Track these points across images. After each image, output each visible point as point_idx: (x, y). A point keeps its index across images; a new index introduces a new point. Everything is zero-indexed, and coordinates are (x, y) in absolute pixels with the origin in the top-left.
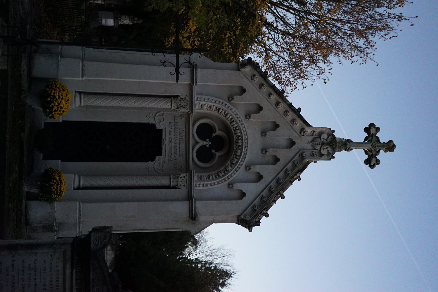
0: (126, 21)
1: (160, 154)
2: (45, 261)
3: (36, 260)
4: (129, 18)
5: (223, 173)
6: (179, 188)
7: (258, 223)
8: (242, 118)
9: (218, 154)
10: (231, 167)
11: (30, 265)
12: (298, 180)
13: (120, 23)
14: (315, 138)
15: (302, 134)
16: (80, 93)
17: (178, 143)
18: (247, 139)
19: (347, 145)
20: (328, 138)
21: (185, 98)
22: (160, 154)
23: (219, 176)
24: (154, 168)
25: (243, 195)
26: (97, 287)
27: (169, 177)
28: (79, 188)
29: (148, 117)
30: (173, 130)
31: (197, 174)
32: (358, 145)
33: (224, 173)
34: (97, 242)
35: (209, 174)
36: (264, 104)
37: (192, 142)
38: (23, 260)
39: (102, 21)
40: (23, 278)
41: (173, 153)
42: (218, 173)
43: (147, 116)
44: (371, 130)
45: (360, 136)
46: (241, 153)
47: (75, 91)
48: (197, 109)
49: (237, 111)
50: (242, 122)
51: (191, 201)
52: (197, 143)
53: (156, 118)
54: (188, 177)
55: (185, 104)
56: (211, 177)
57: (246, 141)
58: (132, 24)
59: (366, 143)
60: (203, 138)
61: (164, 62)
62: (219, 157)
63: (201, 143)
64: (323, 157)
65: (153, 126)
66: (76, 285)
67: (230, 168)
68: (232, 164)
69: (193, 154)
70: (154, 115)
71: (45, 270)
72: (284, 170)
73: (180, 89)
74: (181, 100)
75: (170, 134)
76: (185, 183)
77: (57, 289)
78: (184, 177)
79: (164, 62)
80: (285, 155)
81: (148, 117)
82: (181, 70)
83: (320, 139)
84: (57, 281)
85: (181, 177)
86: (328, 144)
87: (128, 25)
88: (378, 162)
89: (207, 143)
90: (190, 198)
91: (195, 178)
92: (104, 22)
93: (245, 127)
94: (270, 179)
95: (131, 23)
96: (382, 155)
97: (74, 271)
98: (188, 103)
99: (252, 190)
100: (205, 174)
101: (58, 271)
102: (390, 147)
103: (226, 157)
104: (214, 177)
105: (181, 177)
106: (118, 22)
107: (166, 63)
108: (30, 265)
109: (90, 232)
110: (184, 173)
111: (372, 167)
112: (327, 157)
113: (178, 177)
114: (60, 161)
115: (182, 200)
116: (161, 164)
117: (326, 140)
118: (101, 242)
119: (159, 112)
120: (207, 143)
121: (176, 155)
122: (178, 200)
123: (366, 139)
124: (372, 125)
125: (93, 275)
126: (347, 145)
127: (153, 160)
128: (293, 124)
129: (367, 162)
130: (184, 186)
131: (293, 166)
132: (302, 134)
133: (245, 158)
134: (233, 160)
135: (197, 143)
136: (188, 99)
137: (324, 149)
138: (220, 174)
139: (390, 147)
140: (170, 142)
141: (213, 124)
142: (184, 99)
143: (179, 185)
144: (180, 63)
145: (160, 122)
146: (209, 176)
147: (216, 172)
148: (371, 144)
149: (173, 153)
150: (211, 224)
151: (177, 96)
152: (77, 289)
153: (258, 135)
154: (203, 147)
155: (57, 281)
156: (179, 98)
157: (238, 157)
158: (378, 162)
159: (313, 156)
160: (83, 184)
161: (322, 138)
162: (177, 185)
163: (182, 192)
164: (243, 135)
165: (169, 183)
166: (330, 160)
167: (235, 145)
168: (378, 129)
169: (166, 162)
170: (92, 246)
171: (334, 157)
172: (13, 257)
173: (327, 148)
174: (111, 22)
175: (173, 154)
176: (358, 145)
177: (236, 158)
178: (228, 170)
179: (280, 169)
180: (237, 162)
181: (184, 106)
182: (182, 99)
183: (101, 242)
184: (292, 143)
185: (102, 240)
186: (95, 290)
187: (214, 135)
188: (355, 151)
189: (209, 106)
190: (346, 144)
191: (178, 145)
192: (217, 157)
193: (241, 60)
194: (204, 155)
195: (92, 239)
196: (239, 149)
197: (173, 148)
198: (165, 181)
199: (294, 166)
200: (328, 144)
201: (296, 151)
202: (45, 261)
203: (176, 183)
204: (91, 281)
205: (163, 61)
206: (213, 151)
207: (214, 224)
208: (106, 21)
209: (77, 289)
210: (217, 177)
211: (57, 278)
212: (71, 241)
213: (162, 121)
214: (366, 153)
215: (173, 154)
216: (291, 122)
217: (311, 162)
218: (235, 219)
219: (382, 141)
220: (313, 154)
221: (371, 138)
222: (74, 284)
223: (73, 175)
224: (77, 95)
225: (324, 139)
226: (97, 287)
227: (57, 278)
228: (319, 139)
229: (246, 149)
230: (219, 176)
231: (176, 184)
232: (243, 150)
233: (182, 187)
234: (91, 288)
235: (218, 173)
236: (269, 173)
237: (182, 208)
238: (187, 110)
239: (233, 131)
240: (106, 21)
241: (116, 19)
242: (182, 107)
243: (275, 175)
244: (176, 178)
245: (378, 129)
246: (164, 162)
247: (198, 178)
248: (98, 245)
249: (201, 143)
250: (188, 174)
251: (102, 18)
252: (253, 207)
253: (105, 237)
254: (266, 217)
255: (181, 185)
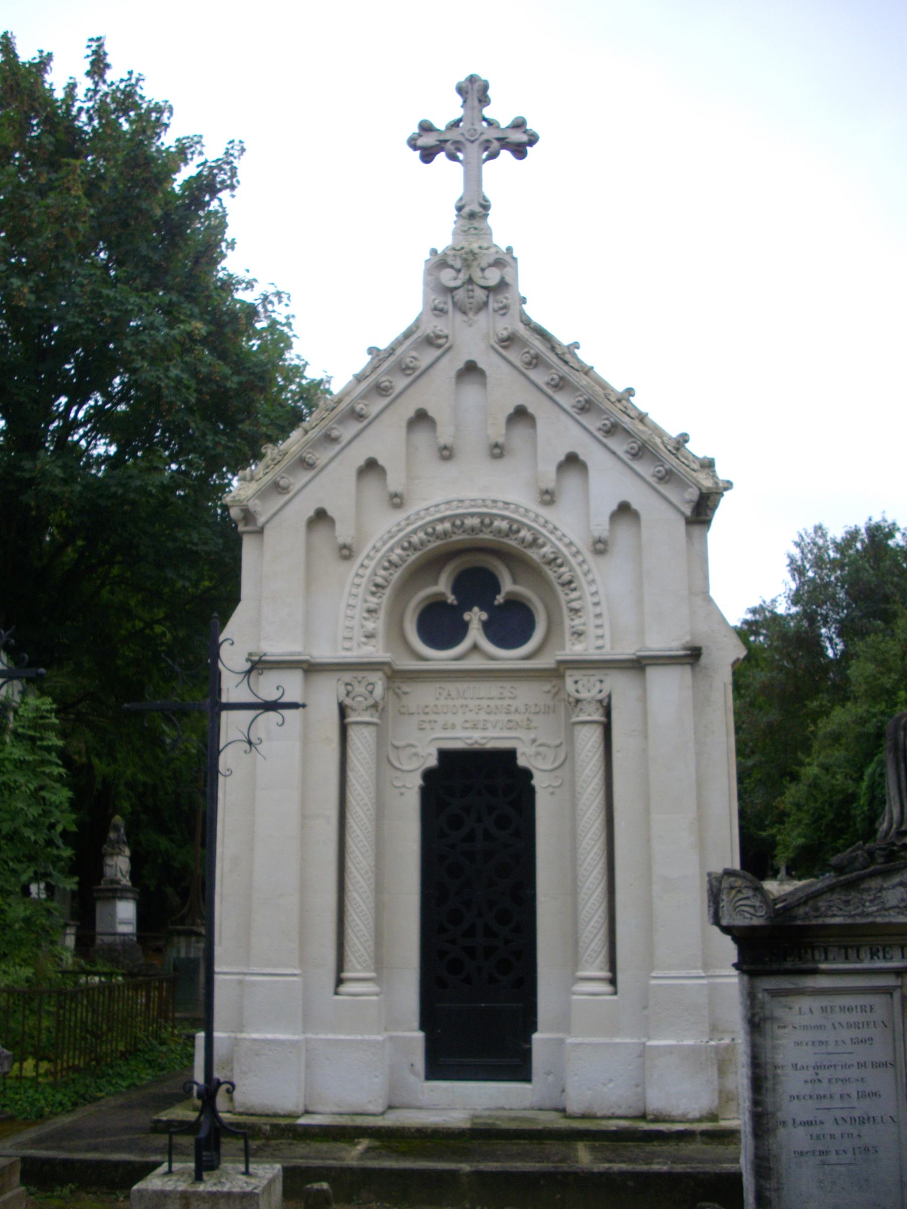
0: (120, 865)
1: (511, 754)
2: (798, 1044)
3: (795, 1067)
4: (112, 855)
5: (563, 569)
6: (609, 697)
7: (708, 465)
8: (399, 516)
9: (508, 586)
10: (543, 546)
11: (806, 1082)
12: (578, 348)
13: (126, 881)
14: (455, 304)
15: (441, 341)
16: (340, 981)
17: (478, 702)
18: (462, 501)
19: (473, 212)
20: (452, 267)
21: (347, 684)
22: (511, 754)
23: (570, 582)
24: (551, 771)
25: (624, 510)
26: (867, 904)
27: (578, 727)
28: (613, 981)
29: (403, 790)
30: (441, 719)
31: (568, 644)
32: (473, 180)
33: (561, 566)
34: (743, 908)
35: (565, 611)
36: (357, 456)
37: (475, 663)
38: (792, 1097)
39: (124, 935)
40: (841, 1096)
41: (505, 718)
42: (563, 585)
43: (402, 794)
44: (429, 145)
45: (447, 173)
46: (504, 518)
47: (336, 993)
48: (375, 651)
49: (382, 533)
50: (412, 518)
51: (644, 662)
52: (475, 647)
53: (405, 767)
54: (575, 672)
55: (364, 683)
56: (576, 605)
57: (467, 503)
58: (129, 847)
59: (466, 157)
60: (459, 631)
61: (250, 743)
62: (515, 582)
63: (475, 634)
64: (508, 279)
65: (428, 775)
66: (861, 961)
67: (546, 550)
68: (534, 543)
69: (510, 657)
70: (399, 774)
71: (821, 1043)
72: (550, 391)
73: (326, 695)
74: (351, 695)
75: (453, 726)
76: (592, 679)
77: (871, 1008)
78: (576, 682)
79: (250, 743)
80: (506, 387)
81: (403, 790)
82: (270, 695)
83: (456, 288)
84: (850, 1009)
85: (577, 691)
86: (472, 278)
87: (133, 860)
88: (519, 124)
89: (476, 617)
90: (638, 665)
91: (575, 650)
92: (129, 929)
93: (427, 509)
94: (576, 430)
95: (127, 852)
96: (500, 112)
97: (823, 966)
98: (360, 675)
99: (610, 481)
100: (567, 623)
101: (824, 1009)
102: (474, 91)
103: (515, 560)
104: (574, 595)
105: (577, 691)
106: (125, 889)
107: (253, 740)
108: (806, 1082)
109: (726, 930)
110: (564, 684)
111: (533, 140)
112: (508, 269)
113: (578, 701)
114: (536, 1036)
115: (644, 689)
116: (541, 749)
117: (459, 271)
118: (747, 898)
119: (389, 761)
120: (476, 617)
121: (513, 709)
122: (643, 699)
123: (453, 157)
124: (413, 144)
125: (834, 916)
126: (473, 212)
127: (527, 775)
128: (414, 369)
129: (519, 151)
130: (601, 681)
131: (536, 366)
132: (441, 341)
133: (518, 506)
134: (523, 540)
135: (475, 647)
136: (347, 677)
137: (484, 278)
138: (566, 577)
139: (474, 91)
140: (475, 727)
141: (418, 605)
142: (349, 688)
143: (600, 696)
144: (248, 698)
145: (416, 754)
146: (572, 610)
147: (559, 589)
148: (468, 145)
149: (505, 718)
150: (710, 600)
151: (343, 711)
152: (872, 958)
153: (449, 470)
154: (487, 627)
155: (850, 1009)
156: (348, 702)
157: (515, 527)
158: (519, 124)
159: (505, 307)
160: (601, 969)
161: (452, 284)
162: (601, 701)
163: (620, 687)
164: (448, 513)
165: (595, 726)
166: (515, 259)
167: (481, 536)
168: (426, 128)
169: (532, 736)
170: (756, 922)
171: (509, 250)
172: (784, 1123)
173: (483, 270)
174: (126, 912)
175: (512, 717)
176: (473, 180)
177: (518, 531)
178: (552, 556)
179: (548, 404)
180: (530, 528)
181: (370, 687)
182: (348, 694)
183: (747, 898)
184: (471, 370)
185: (741, 896)
186: (874, 908)
187: (451, 599)
188: (488, 190)
189: (366, 615)
190: (472, 216)
191: (485, 703)
192: (519, 589)
193: (93, 472)
194: (511, 624)
195: (740, 921)
196: (491, 523)
197: (492, 718)
198: (589, 740)
199: (536, 361)
200: (472, 278)
201: (495, 358)
202: (798, 1044)
203: (594, 706)
204: (849, 921)
205: (247, 746)
206: (500, 599)
207: (713, 593)
208: (124, 923)
209: (872, 958)
210: (573, 586)
211: (842, 1009)
212: (746, 978)
213: (413, 750)
214: (493, 156)
215: (512, 717)
216: (409, 375)
217: (522, 314)
218: (696, 530)
219: (458, 113)
220: (501, 309)
221: (448, 144)
222: (858, 966)
223: (575, 997)
224: (344, 988)
225: (455, 279)
226: (867, 904)
227: (842, 1009)
228: (456, 292)
229: (489, 503)
230: (570, 582)
231: (598, 705)
232: (495, 511)
233: (606, 688)
234: (870, 920)
235: (563, 585)
236: (559, 432)
237: (667, 688)
238: (378, 680)
239: (439, 543)
240: (124, 923)
241: (115, 893)
242: (371, 692)
243: (564, 417)
244: (580, 705)
245: (426, 128)
246: (534, 741)
247: (580, 642)
248: (754, 907)
249: (475, 634)
250: (568, 673)
251: (115, 934)
252: (661, 479)
253: (732, 888)
254: (686, 441)
255: (601, 691)
